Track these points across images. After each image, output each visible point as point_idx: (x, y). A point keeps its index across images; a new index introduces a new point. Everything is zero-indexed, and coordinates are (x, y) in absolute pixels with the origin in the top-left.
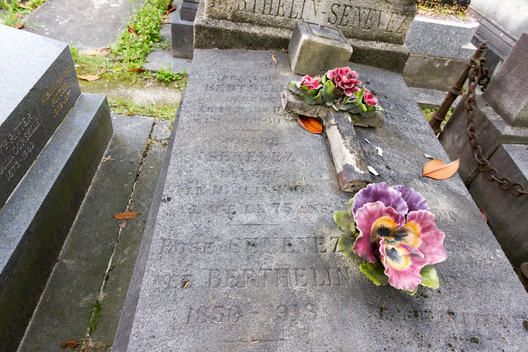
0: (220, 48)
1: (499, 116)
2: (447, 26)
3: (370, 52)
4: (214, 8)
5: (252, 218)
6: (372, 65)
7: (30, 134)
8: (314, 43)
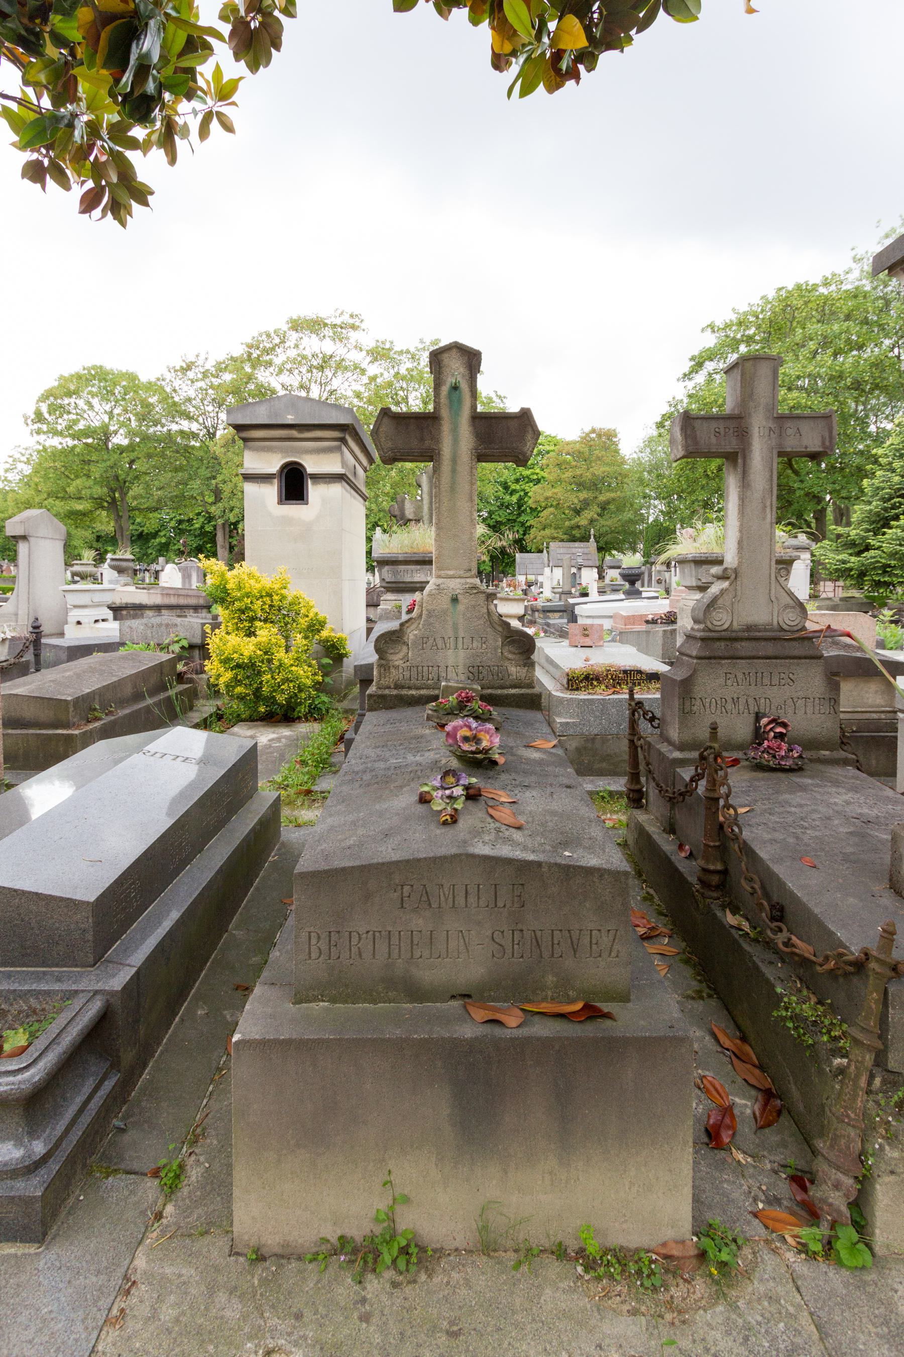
0: (387, 709)
8: (451, 687)
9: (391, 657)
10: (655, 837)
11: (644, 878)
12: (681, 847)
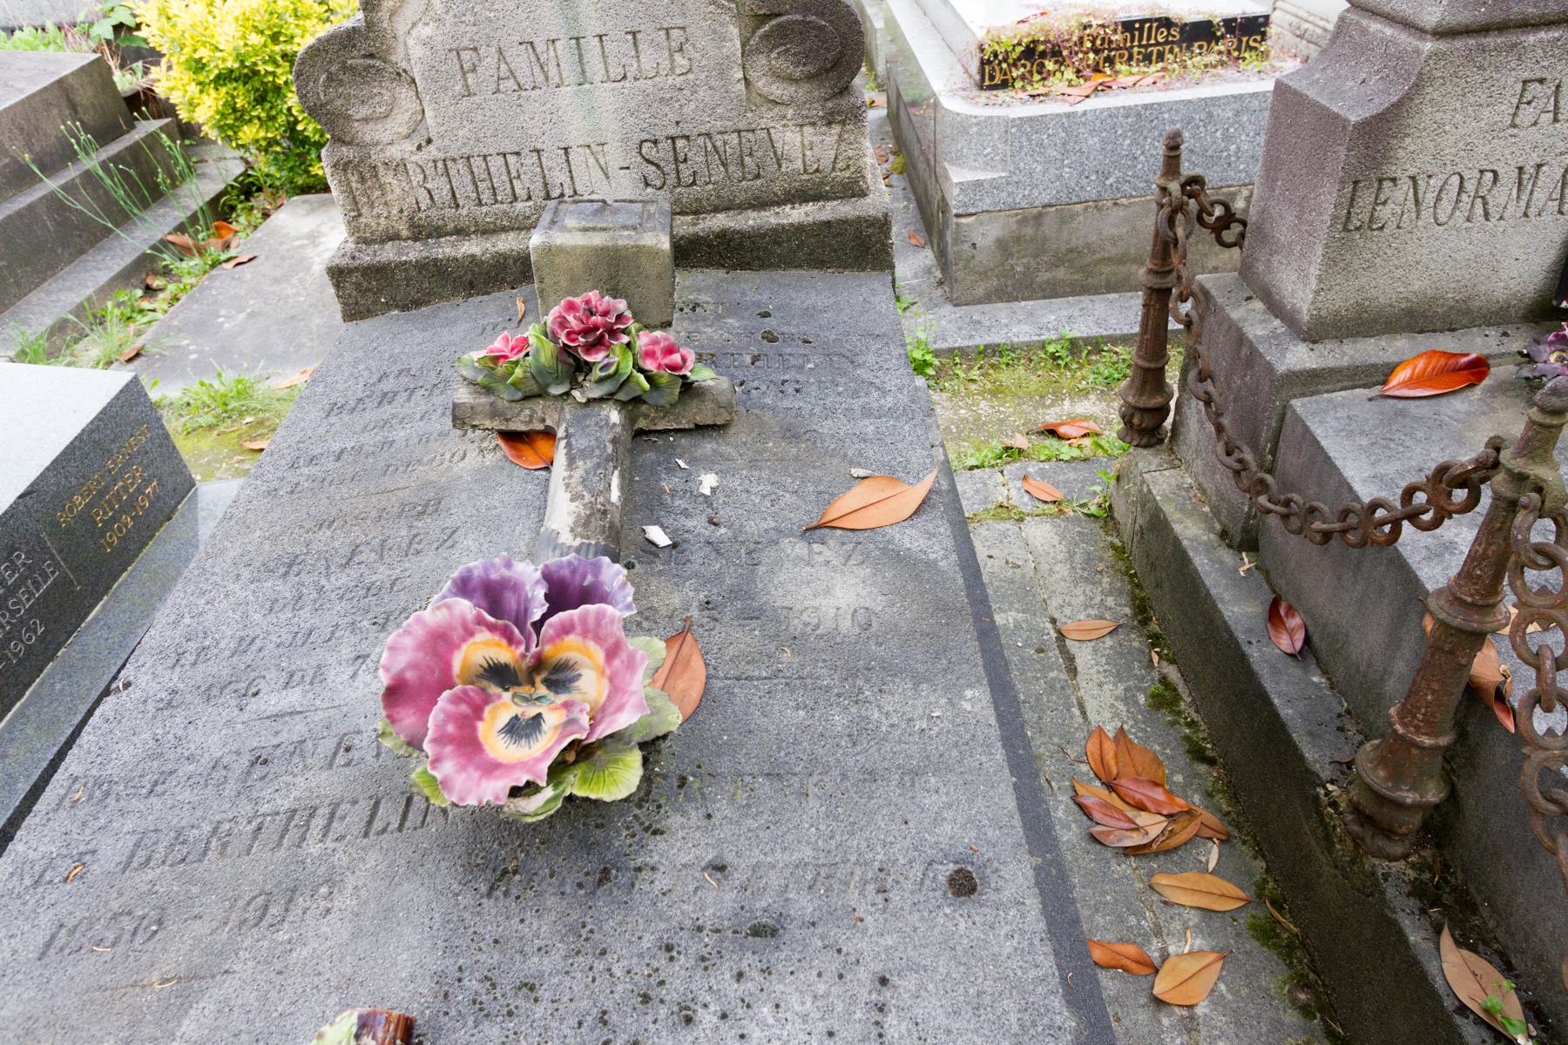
0: (404, 308)
1: (1277, 322)
2: (1200, 100)
3: (777, 235)
4: (362, 220)
5: (293, 698)
6: (799, 266)
7: (28, 600)
8: (561, 250)
9: (368, 133)
10: (1200, 561)
11: (1154, 627)
12: (1274, 615)
